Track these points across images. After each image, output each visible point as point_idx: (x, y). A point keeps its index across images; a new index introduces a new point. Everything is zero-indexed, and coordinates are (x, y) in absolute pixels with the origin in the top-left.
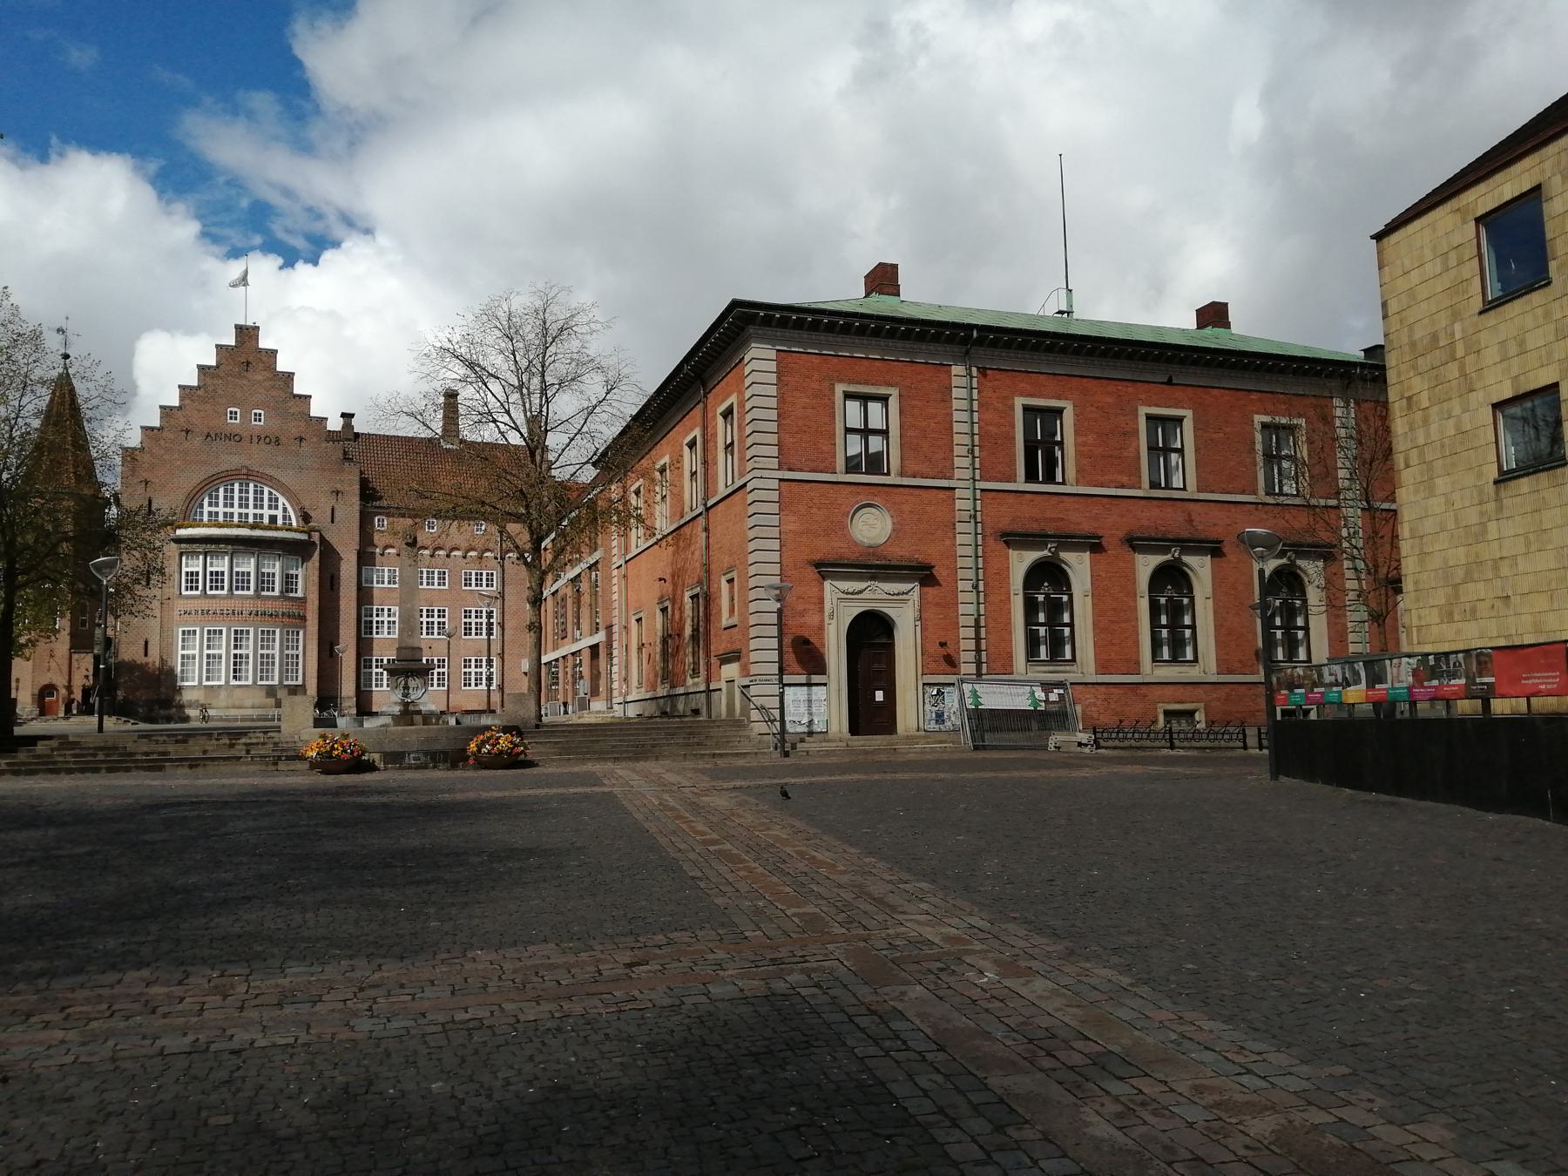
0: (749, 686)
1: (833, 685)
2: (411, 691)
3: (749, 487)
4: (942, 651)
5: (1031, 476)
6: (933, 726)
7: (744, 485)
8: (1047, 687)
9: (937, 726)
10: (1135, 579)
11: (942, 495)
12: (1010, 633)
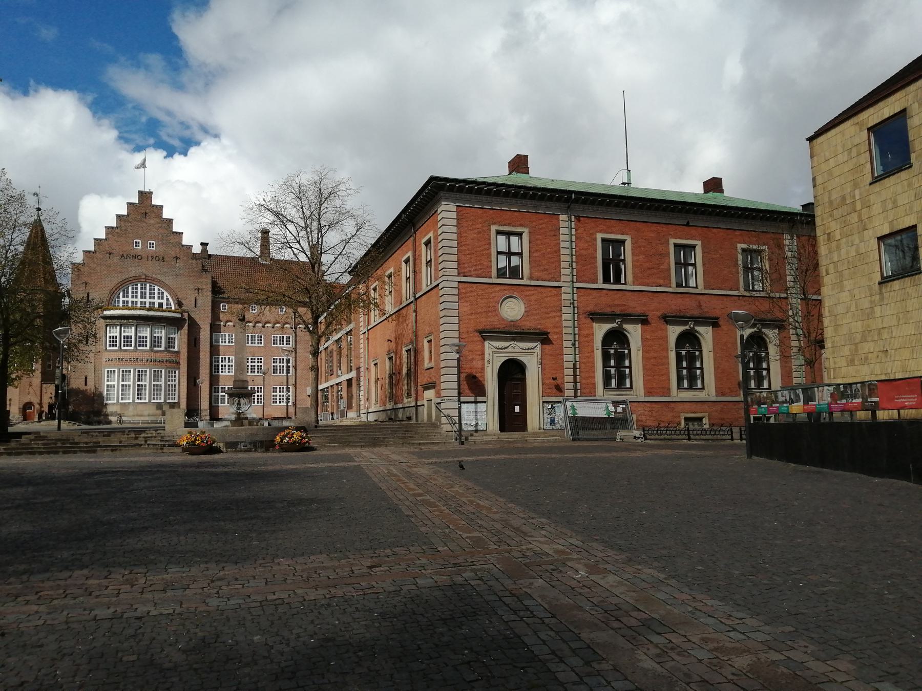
0: (440, 403)
1: (490, 402)
2: (241, 406)
3: (440, 286)
4: (554, 383)
5: (606, 280)
6: (548, 427)
7: (438, 285)
8: (616, 403)
9: (551, 427)
10: (667, 340)
11: (554, 291)
12: (594, 372)
